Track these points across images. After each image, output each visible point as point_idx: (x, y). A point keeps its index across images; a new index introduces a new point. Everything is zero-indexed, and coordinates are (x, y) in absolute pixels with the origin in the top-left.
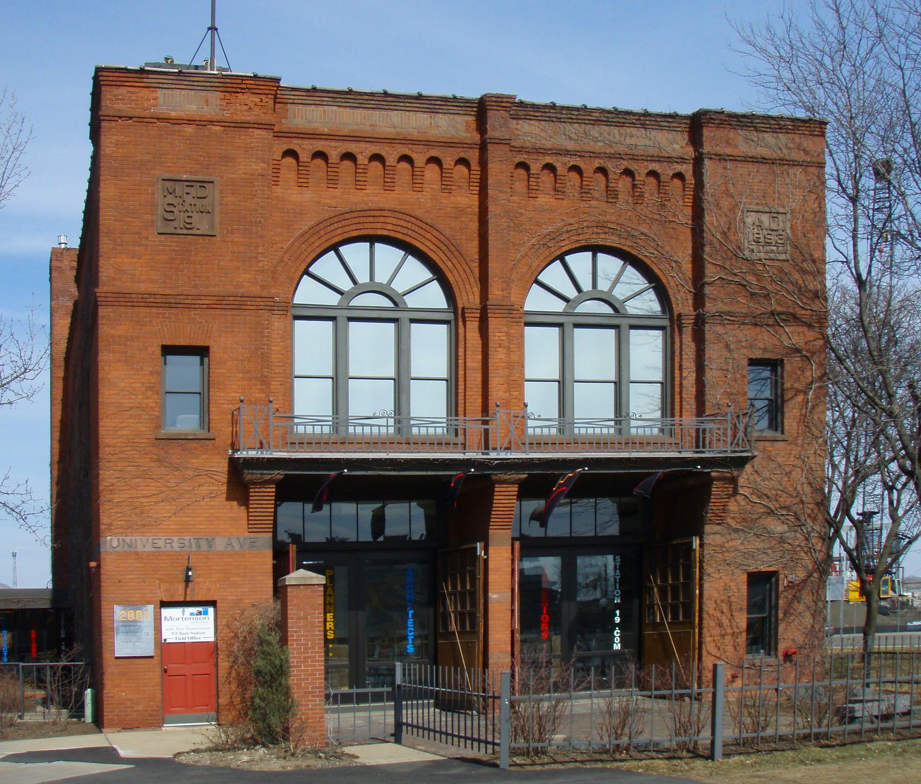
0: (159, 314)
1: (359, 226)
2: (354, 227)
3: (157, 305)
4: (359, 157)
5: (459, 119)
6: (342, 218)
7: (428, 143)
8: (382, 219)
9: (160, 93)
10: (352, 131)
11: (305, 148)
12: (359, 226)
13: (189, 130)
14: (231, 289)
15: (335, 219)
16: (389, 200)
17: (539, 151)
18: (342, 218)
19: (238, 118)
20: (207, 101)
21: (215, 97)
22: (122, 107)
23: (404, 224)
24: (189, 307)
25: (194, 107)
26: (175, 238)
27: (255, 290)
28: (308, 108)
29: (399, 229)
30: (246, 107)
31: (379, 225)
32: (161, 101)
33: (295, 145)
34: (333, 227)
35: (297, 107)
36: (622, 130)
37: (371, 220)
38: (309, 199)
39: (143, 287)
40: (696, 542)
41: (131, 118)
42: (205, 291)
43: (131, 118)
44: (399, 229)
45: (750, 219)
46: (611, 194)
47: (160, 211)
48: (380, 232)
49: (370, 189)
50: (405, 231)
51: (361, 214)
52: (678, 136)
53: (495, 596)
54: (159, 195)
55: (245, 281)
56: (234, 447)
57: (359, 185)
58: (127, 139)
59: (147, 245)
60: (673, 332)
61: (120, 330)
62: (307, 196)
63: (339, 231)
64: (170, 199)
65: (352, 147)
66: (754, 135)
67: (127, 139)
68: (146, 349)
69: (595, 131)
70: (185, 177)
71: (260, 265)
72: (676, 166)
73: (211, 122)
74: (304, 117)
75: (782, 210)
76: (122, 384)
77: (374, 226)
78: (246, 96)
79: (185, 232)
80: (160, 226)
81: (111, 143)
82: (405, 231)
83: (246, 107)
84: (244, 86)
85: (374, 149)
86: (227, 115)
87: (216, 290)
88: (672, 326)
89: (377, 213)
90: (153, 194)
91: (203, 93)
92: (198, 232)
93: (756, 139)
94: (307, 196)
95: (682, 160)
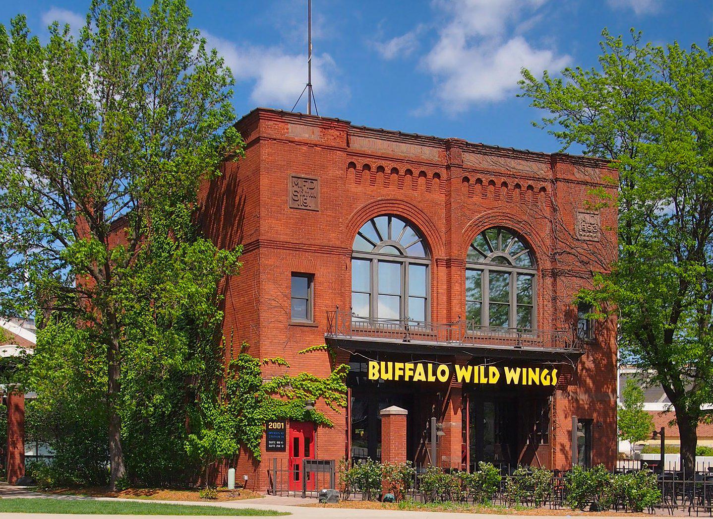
0: (290, 254)
1: (385, 209)
2: (384, 209)
3: (289, 249)
4: (386, 169)
5: (435, 149)
6: (377, 203)
7: (419, 163)
8: (396, 205)
9: (290, 126)
10: (383, 154)
11: (360, 162)
12: (385, 209)
13: (304, 148)
14: (325, 242)
15: (374, 204)
16: (399, 194)
17: (475, 171)
18: (377, 203)
19: (328, 143)
20: (313, 132)
21: (317, 130)
22: (273, 133)
23: (408, 209)
24: (305, 251)
25: (307, 136)
26: (298, 211)
27: (338, 243)
28: (360, 138)
29: (405, 211)
30: (333, 138)
31: (395, 209)
32: (290, 130)
33: (354, 159)
34: (373, 208)
35: (355, 137)
36: (516, 161)
37: (391, 205)
38: (363, 191)
39: (282, 238)
40: (551, 399)
41: (275, 140)
42: (313, 242)
43: (275, 140)
44: (405, 211)
45: (580, 217)
46: (510, 198)
47: (291, 195)
48: (395, 212)
49: (391, 188)
50: (408, 213)
51: (387, 202)
52: (543, 166)
53: (454, 424)
54: (290, 185)
55: (333, 238)
56: (329, 330)
57: (386, 185)
58: (273, 151)
59: (284, 214)
60: (432, 269)
61: (270, 262)
62: (360, 189)
63: (376, 211)
64: (296, 188)
65: (383, 163)
66: (582, 168)
67: (273, 151)
68: (284, 274)
69: (502, 160)
70: (303, 176)
71: (340, 229)
72: (542, 183)
73: (316, 145)
74: (360, 143)
75: (596, 213)
76: (272, 293)
77: (393, 209)
78: (332, 131)
79: (304, 207)
80: (291, 203)
81: (265, 153)
82: (408, 213)
83: (333, 137)
84: (332, 125)
85: (394, 165)
86: (323, 141)
87: (318, 242)
88: (432, 264)
89: (394, 202)
90: (287, 185)
91: (311, 128)
92: (310, 208)
93: (583, 170)
94: (360, 189)
95: (545, 180)
